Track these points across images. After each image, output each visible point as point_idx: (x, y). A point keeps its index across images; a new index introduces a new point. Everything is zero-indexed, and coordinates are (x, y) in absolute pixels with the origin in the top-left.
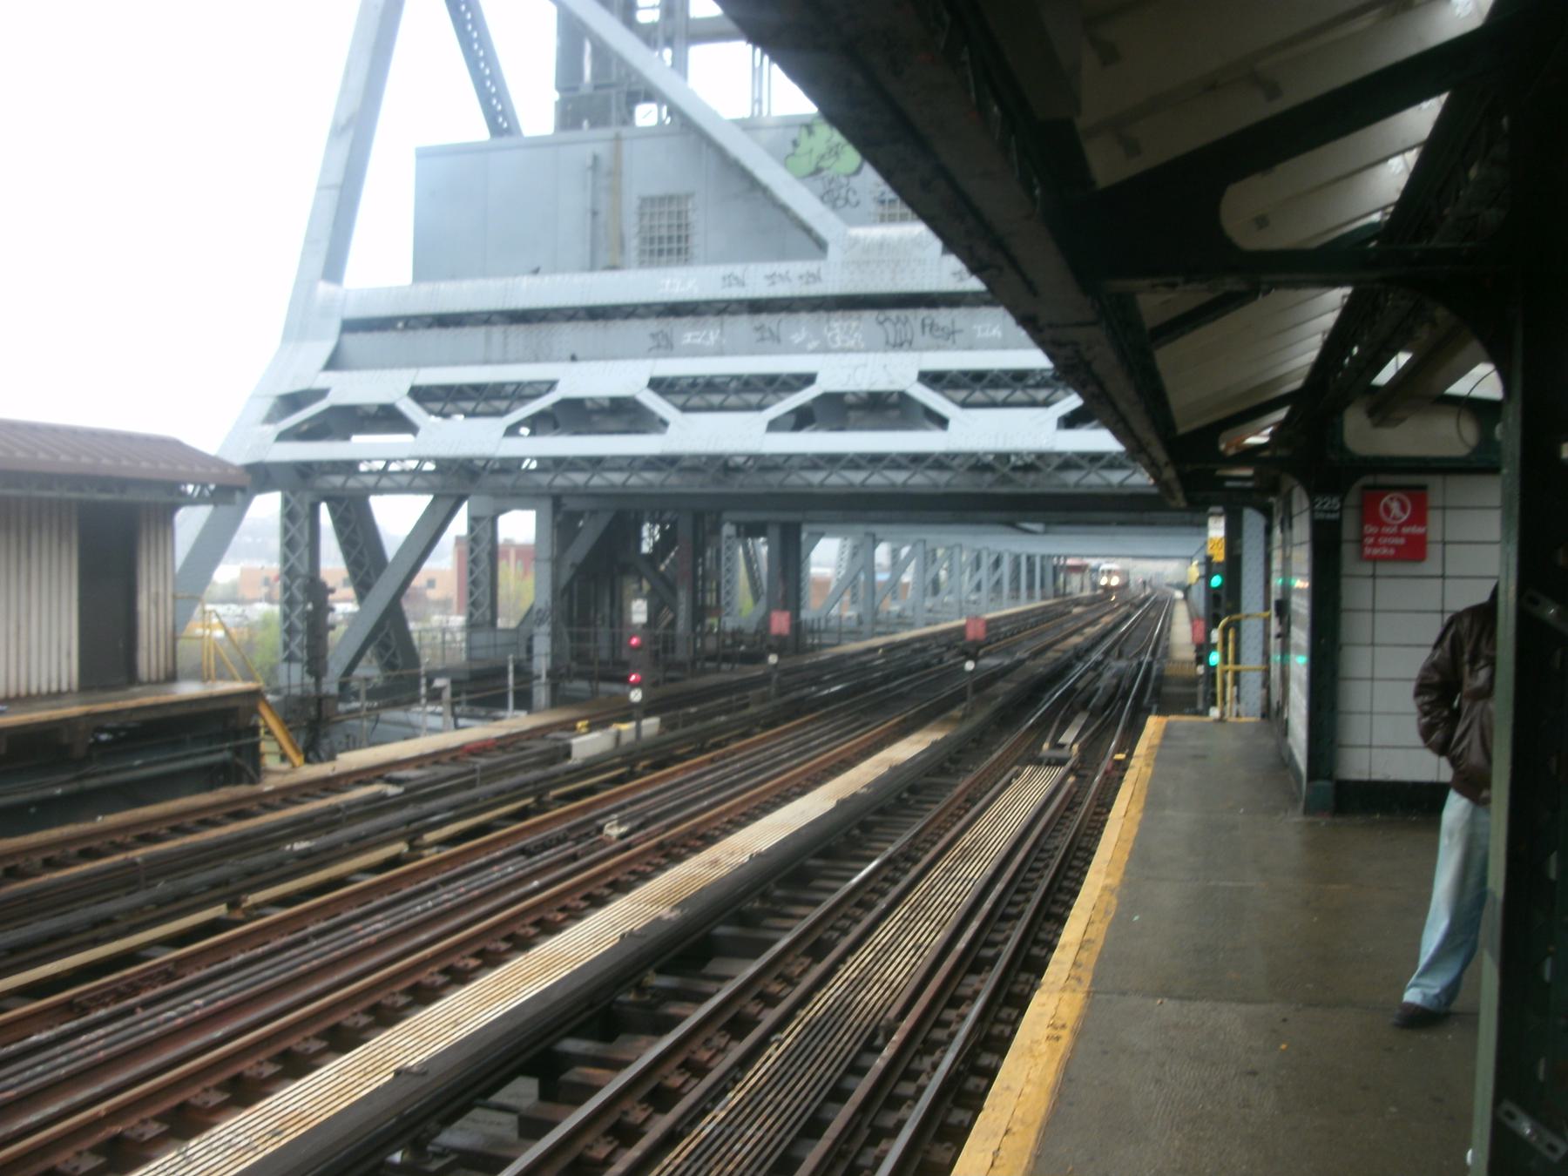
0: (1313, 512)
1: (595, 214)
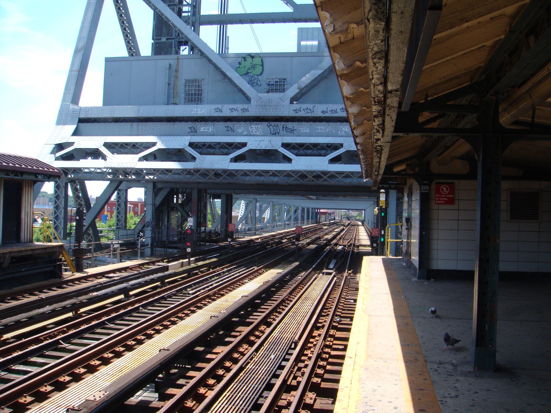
0: (421, 190)
1: (169, 84)
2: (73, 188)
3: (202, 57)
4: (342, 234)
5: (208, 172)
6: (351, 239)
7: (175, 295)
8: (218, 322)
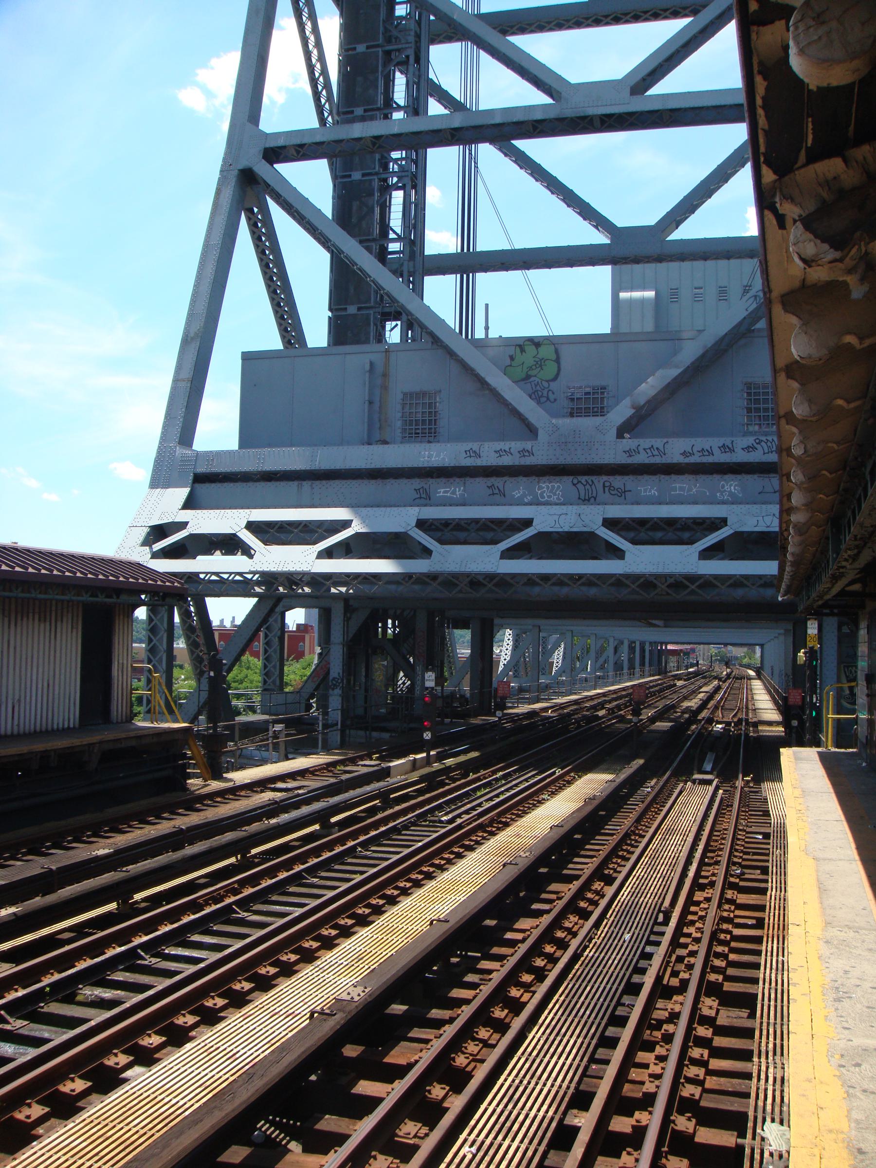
1: (371, 403)
2: (183, 610)
4: (718, 697)
5: (457, 579)
6: (739, 709)
7: (414, 824)
8: (519, 873)
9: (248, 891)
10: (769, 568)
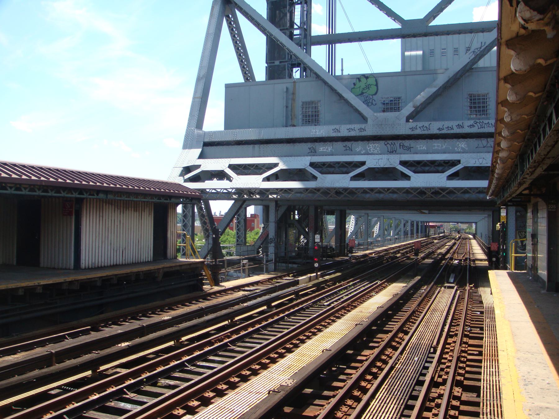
0: (548, 209)
1: (287, 107)
2: (199, 207)
3: (317, 80)
4: (455, 248)
7: (311, 306)
9: (235, 337)
10: (484, 184)
